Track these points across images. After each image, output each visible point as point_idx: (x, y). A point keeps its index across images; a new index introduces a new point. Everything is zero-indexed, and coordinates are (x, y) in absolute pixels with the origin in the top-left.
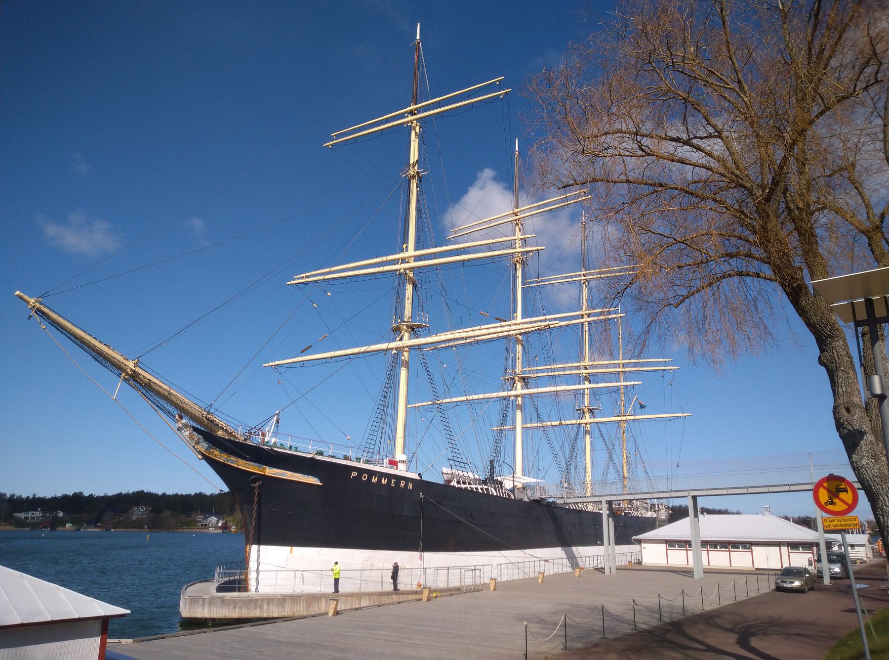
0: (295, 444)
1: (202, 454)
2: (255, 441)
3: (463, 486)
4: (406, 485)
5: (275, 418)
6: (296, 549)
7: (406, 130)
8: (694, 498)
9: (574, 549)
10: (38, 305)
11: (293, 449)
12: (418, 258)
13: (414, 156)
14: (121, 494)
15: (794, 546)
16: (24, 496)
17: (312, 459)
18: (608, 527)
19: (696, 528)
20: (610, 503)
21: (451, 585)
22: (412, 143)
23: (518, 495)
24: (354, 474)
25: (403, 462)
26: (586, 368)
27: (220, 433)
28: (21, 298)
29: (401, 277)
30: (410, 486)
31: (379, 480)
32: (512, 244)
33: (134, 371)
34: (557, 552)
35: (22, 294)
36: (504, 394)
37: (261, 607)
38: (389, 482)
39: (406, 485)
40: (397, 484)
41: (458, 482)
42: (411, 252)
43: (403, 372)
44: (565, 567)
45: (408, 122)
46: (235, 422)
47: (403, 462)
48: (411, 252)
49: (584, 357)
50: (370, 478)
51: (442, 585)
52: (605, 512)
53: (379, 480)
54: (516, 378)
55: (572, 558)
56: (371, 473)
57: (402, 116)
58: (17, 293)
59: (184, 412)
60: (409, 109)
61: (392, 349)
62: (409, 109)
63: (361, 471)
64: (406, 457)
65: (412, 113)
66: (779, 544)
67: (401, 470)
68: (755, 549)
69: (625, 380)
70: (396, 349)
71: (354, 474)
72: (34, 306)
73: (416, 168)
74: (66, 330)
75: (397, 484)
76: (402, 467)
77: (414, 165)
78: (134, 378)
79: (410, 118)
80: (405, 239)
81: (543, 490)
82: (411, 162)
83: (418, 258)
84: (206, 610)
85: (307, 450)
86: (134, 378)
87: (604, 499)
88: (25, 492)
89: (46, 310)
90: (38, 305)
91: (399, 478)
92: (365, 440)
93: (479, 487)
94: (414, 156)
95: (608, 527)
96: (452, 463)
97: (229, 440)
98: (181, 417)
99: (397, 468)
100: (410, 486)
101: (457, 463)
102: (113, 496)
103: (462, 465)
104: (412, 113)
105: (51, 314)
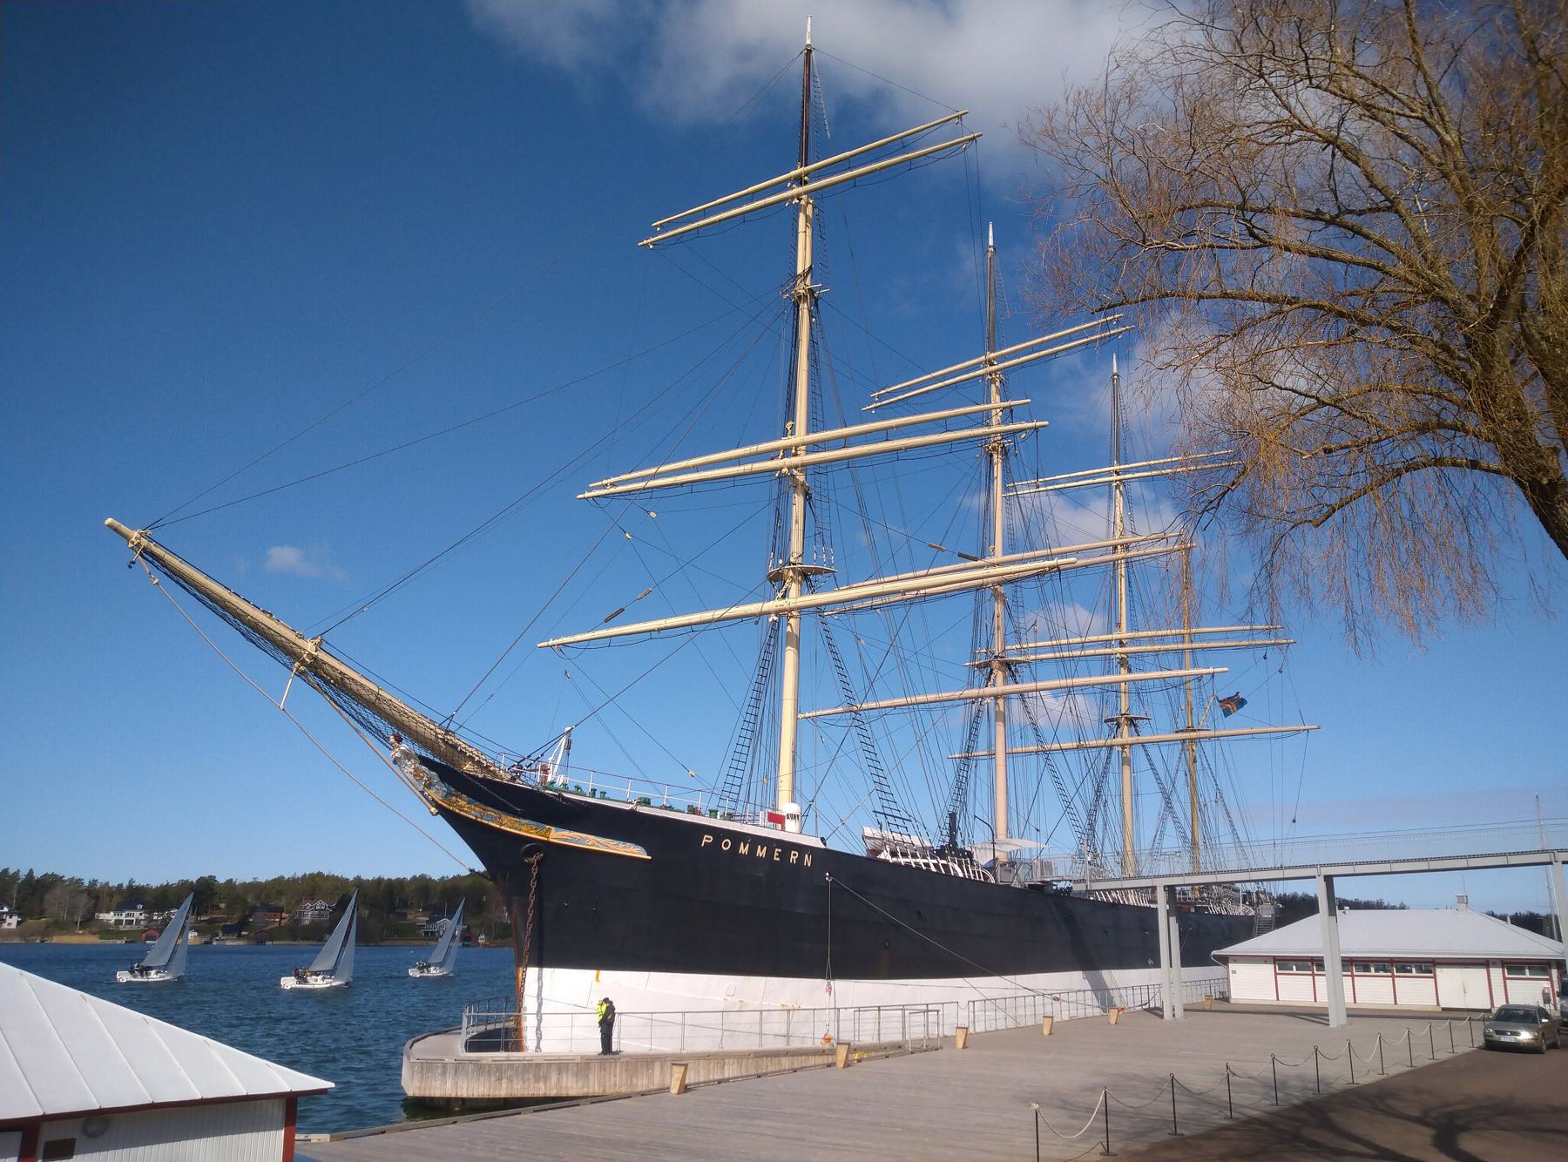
0: (600, 787)
1: (437, 806)
2: (531, 780)
3: (902, 861)
4: (800, 859)
5: (563, 741)
6: (604, 974)
7: (790, 211)
8: (1329, 880)
9: (1105, 974)
10: (144, 542)
11: (598, 794)
12: (813, 447)
13: (803, 261)
14: (320, 874)
15: (1515, 966)
16: (113, 883)
17: (632, 812)
18: (1168, 934)
19: (1333, 936)
20: (1170, 889)
21: (885, 1039)
22: (801, 236)
23: (1002, 877)
24: (707, 839)
25: (794, 817)
26: (1121, 644)
27: (468, 767)
28: (116, 530)
29: (784, 481)
30: (808, 861)
31: (753, 850)
32: (984, 418)
33: (315, 659)
34: (1074, 980)
35: (117, 523)
36: (974, 692)
37: (546, 1078)
38: (770, 853)
39: (800, 859)
40: (785, 855)
41: (894, 854)
42: (801, 435)
43: (790, 655)
44: (1089, 1007)
45: (792, 198)
46: (495, 745)
47: (794, 817)
48: (801, 435)
49: (1119, 625)
50: (735, 847)
51: (867, 1038)
52: (1162, 906)
53: (753, 850)
54: (995, 664)
55: (1100, 990)
56: (738, 837)
57: (781, 187)
58: (109, 521)
59: (403, 730)
60: (793, 173)
61: (769, 613)
62: (793, 173)
63: (719, 834)
64: (808, 805)
65: (799, 180)
66: (1486, 963)
67: (790, 832)
68: (1442, 973)
69: (1195, 665)
70: (777, 613)
71: (707, 839)
72: (138, 545)
73: (808, 281)
74: (196, 587)
75: (785, 855)
76: (791, 825)
77: (805, 275)
78: (314, 670)
79: (797, 190)
80: (790, 413)
81: (1046, 866)
82: (800, 271)
83: (813, 447)
84: (449, 1084)
85: (622, 796)
86: (314, 670)
87: (1160, 884)
88: (115, 875)
89: (158, 551)
90: (144, 542)
91: (787, 847)
92: (723, 778)
93: (932, 862)
94: (803, 261)
95: (1168, 934)
96: (881, 818)
97: (483, 780)
98: (399, 740)
99: (783, 829)
100: (808, 861)
101: (891, 819)
102: (268, 882)
103: (899, 822)
104: (799, 180)
105: (168, 557)
